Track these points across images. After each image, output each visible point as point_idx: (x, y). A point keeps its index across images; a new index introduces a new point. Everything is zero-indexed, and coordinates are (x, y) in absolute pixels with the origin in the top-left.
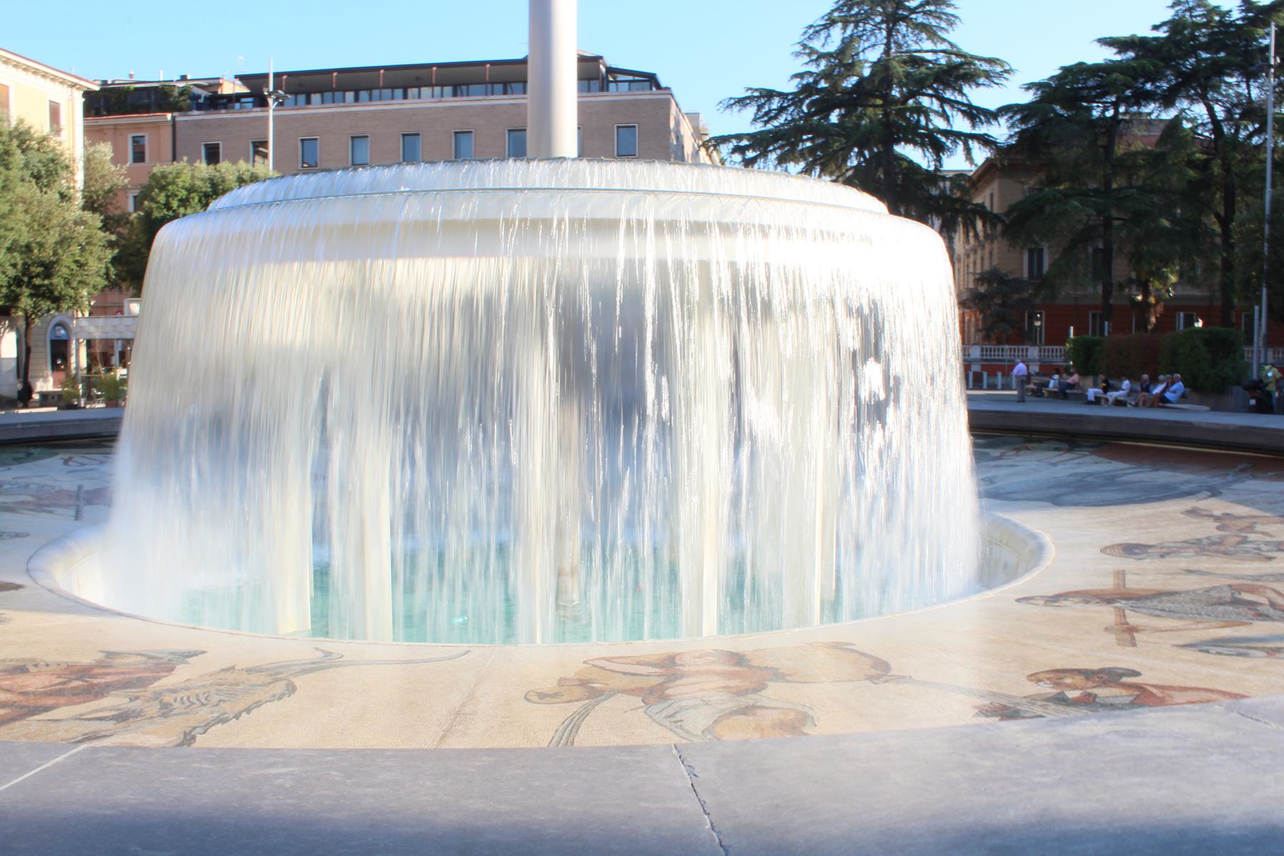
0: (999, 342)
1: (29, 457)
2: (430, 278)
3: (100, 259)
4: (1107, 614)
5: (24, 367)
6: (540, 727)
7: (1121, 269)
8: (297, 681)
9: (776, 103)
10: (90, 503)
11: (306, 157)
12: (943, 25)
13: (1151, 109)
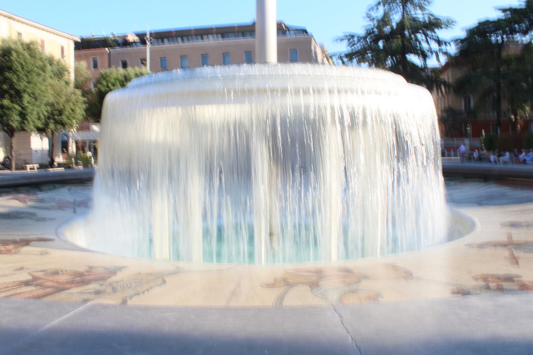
0: (452, 137)
1: (55, 188)
2: (215, 114)
3: (80, 108)
4: (505, 253)
5: (51, 153)
6: (268, 298)
7: (505, 105)
8: (167, 279)
10: (83, 206)
11: (162, 65)
12: (426, 3)
13: (518, 37)
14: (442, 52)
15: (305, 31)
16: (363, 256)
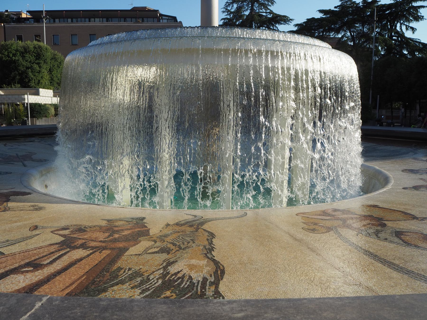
12: (270, 4)
15: (174, 19)
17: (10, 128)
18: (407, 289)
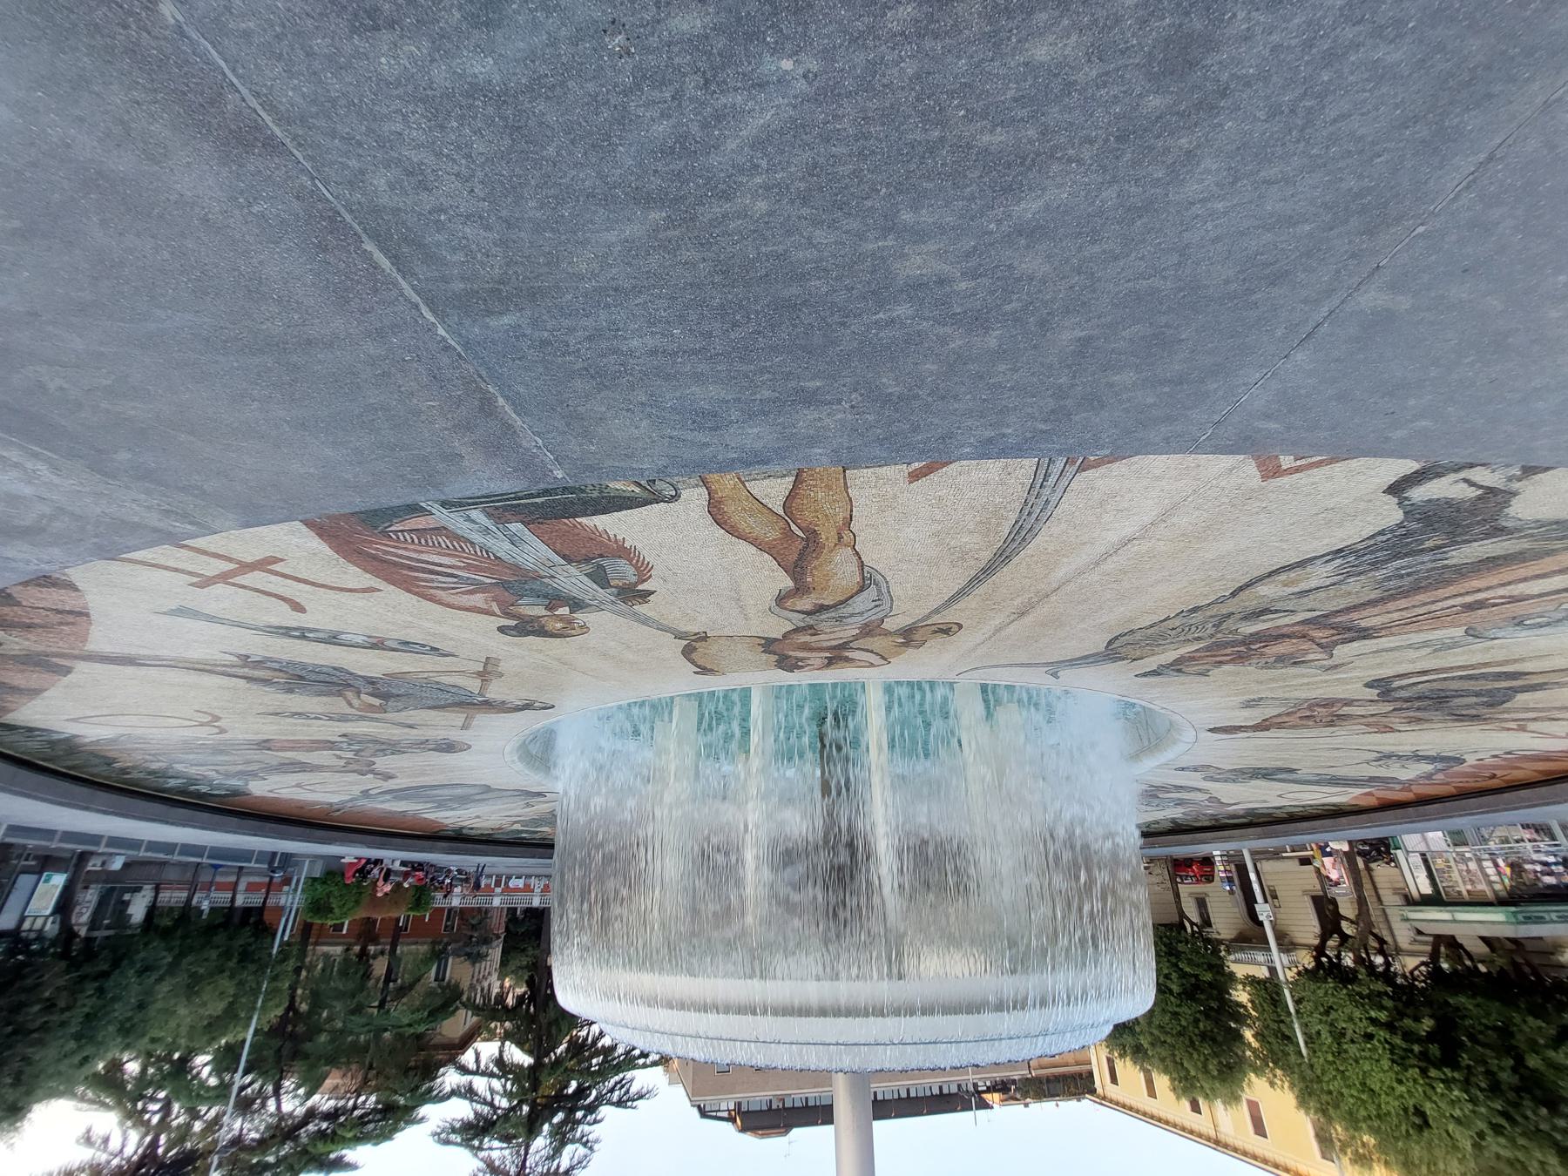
9: (616, 1096)
14: (794, 596)
15: (704, 1113)
16: (87, 615)
17: (1320, 837)
18: (126, 27)
